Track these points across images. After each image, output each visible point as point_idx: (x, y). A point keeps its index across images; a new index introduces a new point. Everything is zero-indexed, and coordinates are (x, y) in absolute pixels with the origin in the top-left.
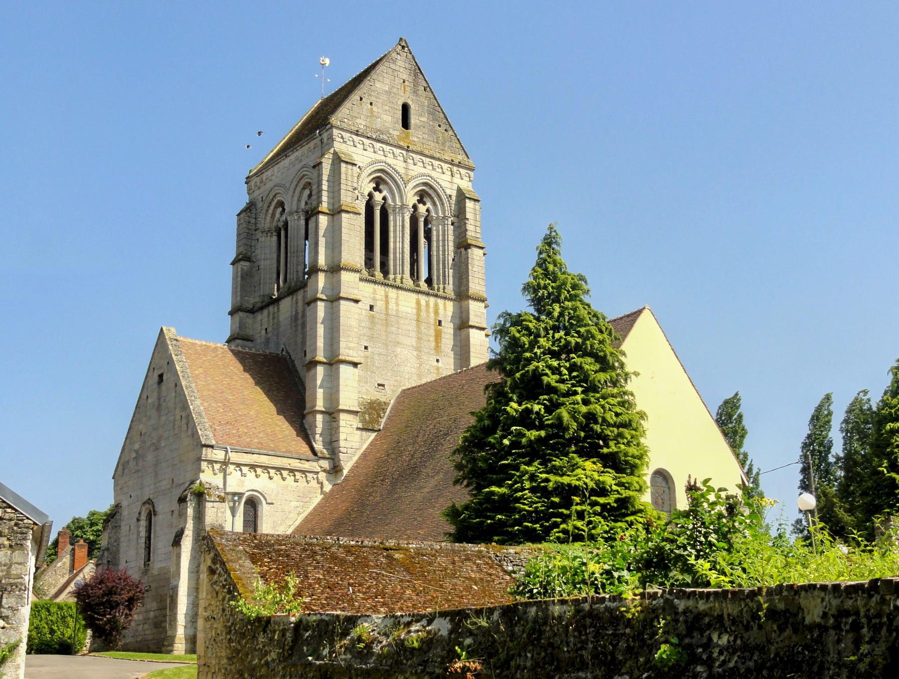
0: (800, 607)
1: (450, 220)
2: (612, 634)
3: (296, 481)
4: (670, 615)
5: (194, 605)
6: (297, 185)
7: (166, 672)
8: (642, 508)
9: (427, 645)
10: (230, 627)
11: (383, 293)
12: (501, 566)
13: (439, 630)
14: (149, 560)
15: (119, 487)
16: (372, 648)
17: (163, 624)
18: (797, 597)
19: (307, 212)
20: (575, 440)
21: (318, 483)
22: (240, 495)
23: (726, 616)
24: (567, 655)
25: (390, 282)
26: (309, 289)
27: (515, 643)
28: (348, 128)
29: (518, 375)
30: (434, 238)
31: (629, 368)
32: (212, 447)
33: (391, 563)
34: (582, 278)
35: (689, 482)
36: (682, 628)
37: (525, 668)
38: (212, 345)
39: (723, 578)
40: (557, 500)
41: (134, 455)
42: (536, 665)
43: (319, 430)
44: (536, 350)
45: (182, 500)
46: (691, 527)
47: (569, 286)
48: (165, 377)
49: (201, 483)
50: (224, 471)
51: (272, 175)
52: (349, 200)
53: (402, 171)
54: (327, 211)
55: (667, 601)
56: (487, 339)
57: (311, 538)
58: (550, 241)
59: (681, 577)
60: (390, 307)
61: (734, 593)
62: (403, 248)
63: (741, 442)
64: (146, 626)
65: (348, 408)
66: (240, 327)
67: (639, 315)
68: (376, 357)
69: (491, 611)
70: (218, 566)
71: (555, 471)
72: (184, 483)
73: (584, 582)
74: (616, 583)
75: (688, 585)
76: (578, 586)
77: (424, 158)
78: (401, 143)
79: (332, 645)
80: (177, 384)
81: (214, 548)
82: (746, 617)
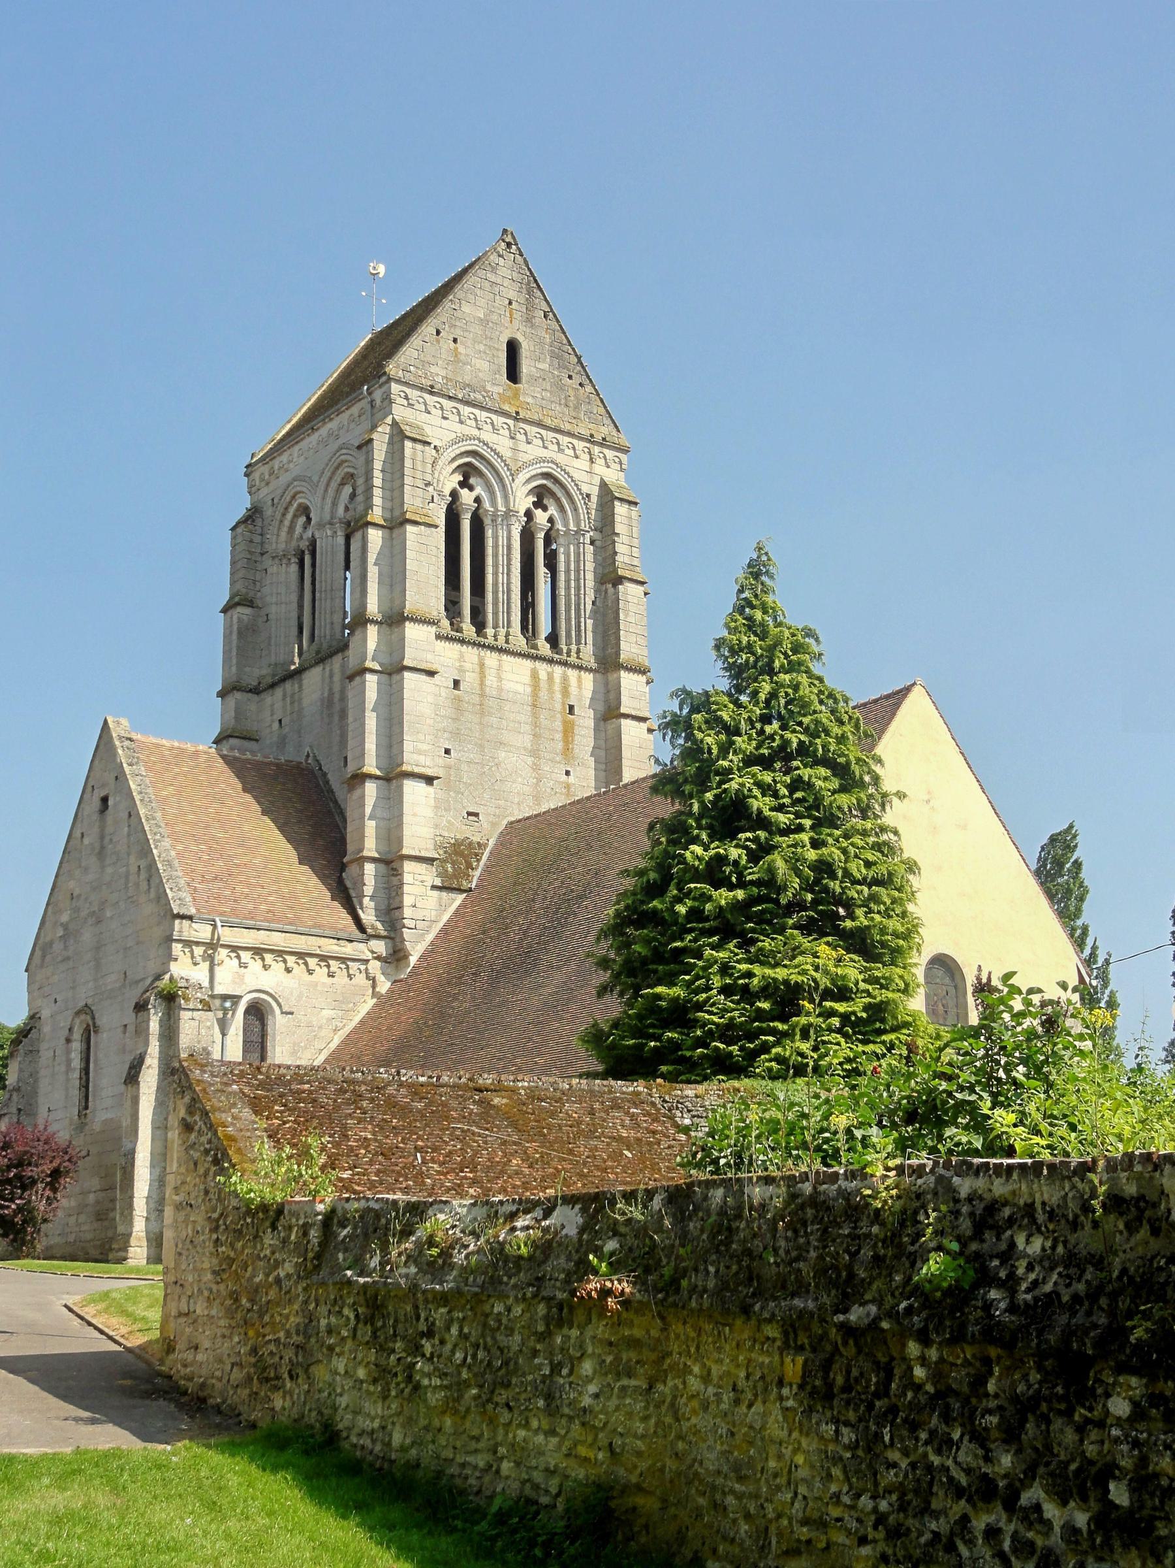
0: (1163, 1192)
1: (588, 536)
2: (849, 1235)
3: (331, 975)
4: (945, 1203)
5: (159, 1182)
6: (331, 478)
7: (114, 1295)
8: (910, 1019)
9: (544, 1252)
10: (217, 1220)
11: (476, 660)
12: (672, 1118)
13: (563, 1226)
14: (86, 1108)
15: (37, 986)
16: (451, 1256)
17: (111, 1215)
18: (1157, 1174)
19: (348, 524)
20: (796, 905)
21: (368, 978)
22: (235, 999)
23: (1038, 1206)
24: (774, 1269)
25: (487, 642)
26: (351, 652)
27: (689, 1248)
28: (417, 382)
29: (709, 796)
30: (561, 566)
31: (888, 786)
32: (190, 918)
33: (487, 1113)
34: (809, 633)
35: (979, 979)
36: (965, 1225)
37: (705, 1290)
38: (189, 747)
39: (1037, 1139)
40: (765, 1005)
41: (60, 933)
42: (723, 1286)
43: (369, 890)
44: (731, 756)
45: (141, 1007)
46: (982, 1052)
47: (787, 645)
48: (110, 803)
49: (171, 978)
50: (211, 959)
51: (290, 462)
52: (418, 502)
53: (507, 454)
54: (382, 522)
55: (940, 1179)
56: (651, 737)
57: (352, 1072)
58: (757, 571)
59: (964, 1139)
60: (488, 683)
61: (1052, 1167)
62: (509, 583)
63: (1079, 910)
64: (82, 1218)
65: (418, 854)
66: (236, 718)
67: (905, 696)
68: (464, 767)
69: (650, 1194)
70: (197, 1118)
71: (760, 958)
72: (143, 979)
73: (804, 1146)
74: (859, 1148)
75: (977, 1153)
76: (794, 1152)
77: (543, 432)
78: (506, 407)
79: (385, 1250)
80: (132, 813)
81: (190, 1087)
82: (1073, 1207)
